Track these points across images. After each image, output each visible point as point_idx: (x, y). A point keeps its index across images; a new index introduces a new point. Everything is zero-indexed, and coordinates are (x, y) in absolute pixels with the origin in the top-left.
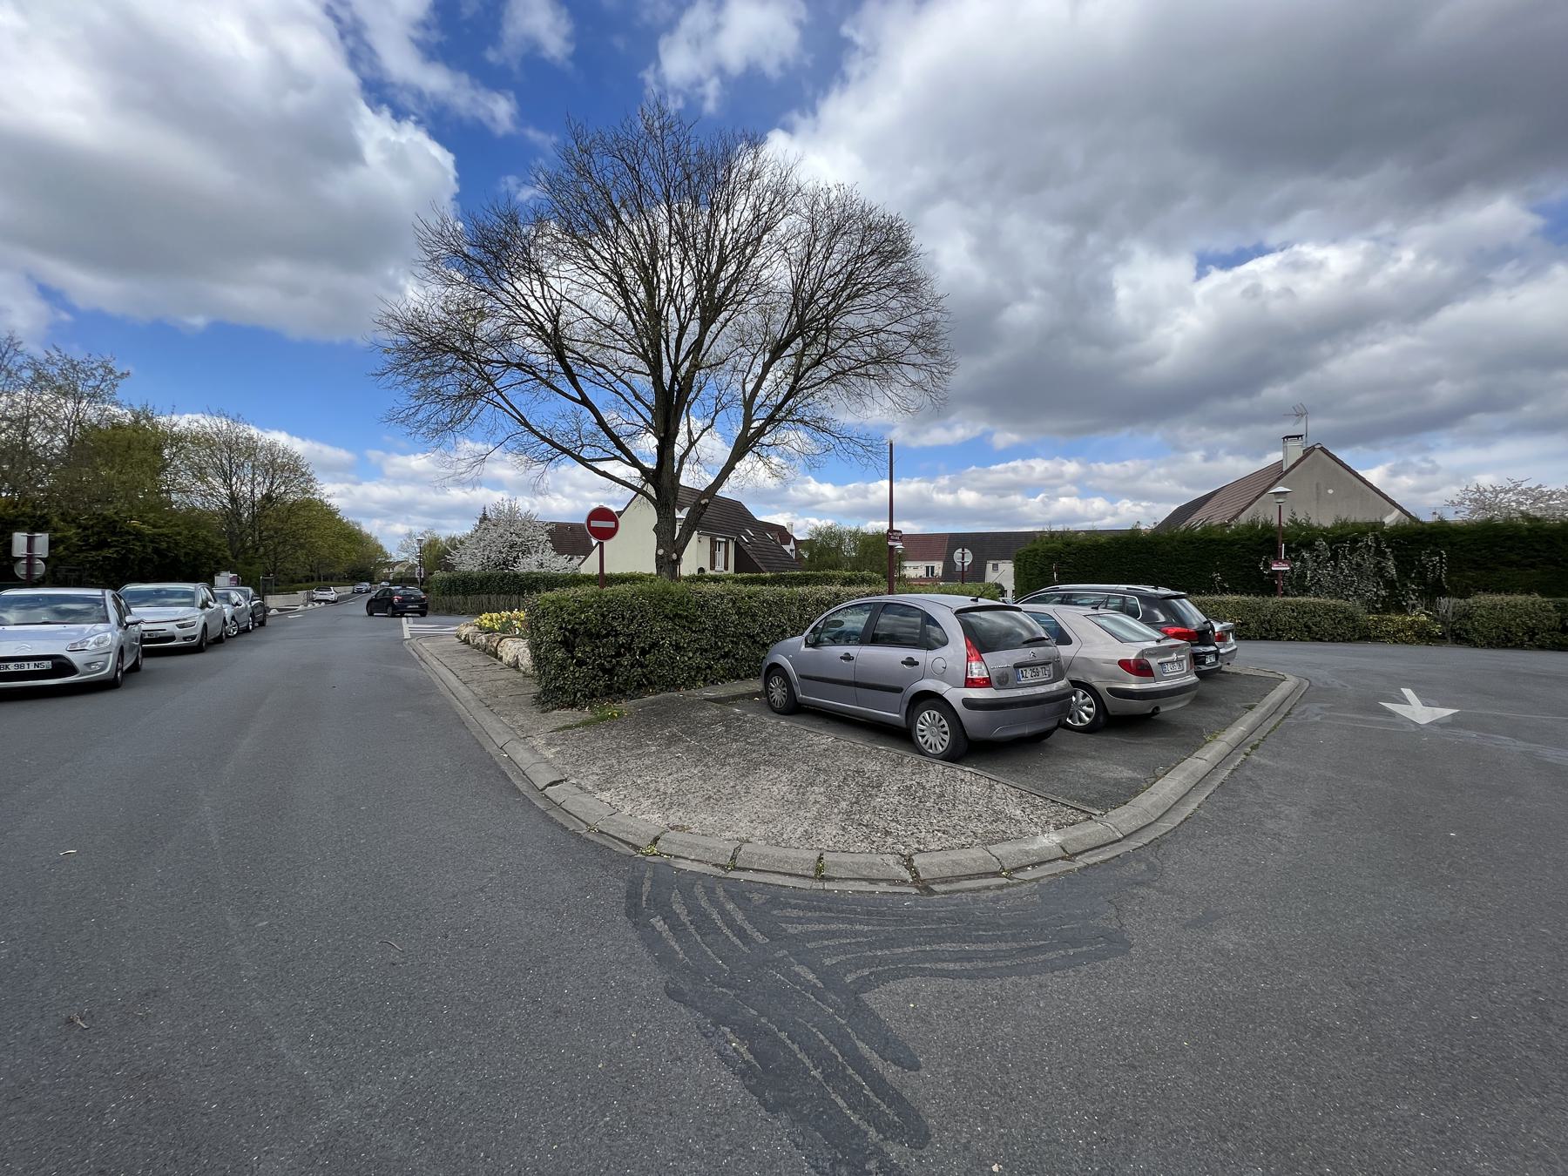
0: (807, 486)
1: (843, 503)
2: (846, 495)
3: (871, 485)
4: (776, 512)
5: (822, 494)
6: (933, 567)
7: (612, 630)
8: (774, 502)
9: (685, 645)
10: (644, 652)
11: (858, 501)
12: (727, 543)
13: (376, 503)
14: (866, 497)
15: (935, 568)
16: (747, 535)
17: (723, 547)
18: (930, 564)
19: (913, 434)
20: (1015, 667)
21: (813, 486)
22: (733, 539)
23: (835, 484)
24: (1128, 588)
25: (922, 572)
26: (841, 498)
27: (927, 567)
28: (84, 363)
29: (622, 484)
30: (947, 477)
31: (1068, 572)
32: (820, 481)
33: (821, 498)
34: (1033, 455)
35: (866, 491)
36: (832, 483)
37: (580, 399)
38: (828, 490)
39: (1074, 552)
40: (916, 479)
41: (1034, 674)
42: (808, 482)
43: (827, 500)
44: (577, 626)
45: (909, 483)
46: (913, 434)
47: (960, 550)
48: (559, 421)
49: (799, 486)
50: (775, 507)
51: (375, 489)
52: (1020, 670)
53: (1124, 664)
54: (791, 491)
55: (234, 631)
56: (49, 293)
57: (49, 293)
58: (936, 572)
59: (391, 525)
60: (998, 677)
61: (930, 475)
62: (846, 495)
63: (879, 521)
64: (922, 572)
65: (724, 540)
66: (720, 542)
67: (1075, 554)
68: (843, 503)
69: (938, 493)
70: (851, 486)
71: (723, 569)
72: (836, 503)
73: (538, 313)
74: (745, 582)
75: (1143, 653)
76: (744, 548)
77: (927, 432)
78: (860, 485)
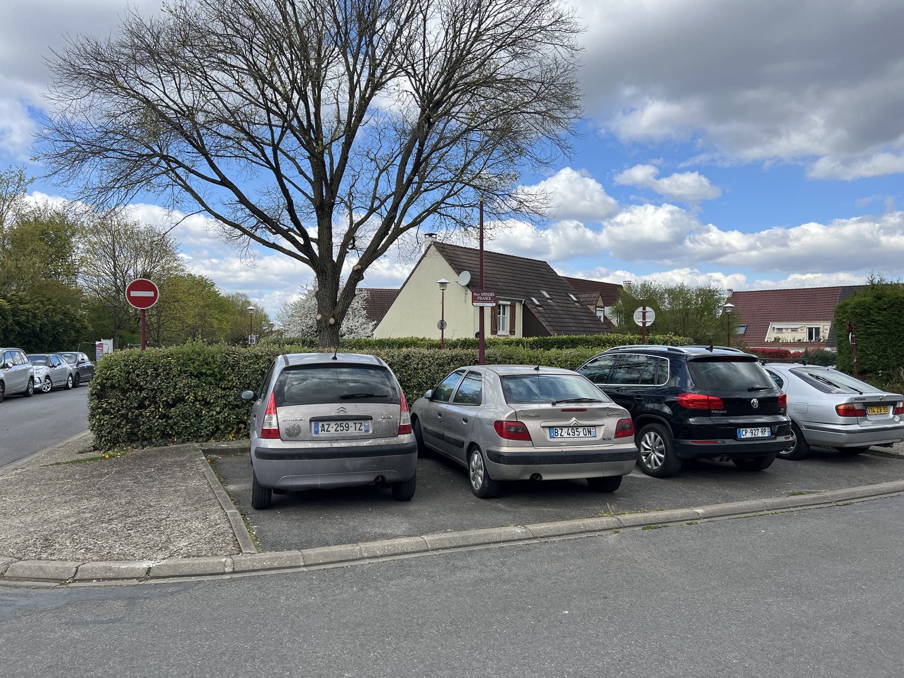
0: (706, 235)
1: (754, 253)
2: (758, 244)
3: (794, 231)
4: (671, 268)
5: (728, 244)
6: (818, 330)
7: (136, 385)
8: (668, 257)
9: (212, 401)
10: (169, 406)
11: (774, 250)
12: (513, 307)
13: (276, 275)
14: (785, 245)
15: (821, 330)
16: (541, 298)
17: (508, 310)
18: (814, 325)
19: (846, 163)
20: (311, 421)
21: (715, 235)
22: (521, 302)
23: (744, 231)
24: (669, 349)
25: (803, 336)
26: (752, 248)
27: (810, 330)
28: (7, 173)
29: (287, 254)
30: (898, 213)
31: (879, 333)
32: (725, 227)
33: (726, 249)
34: (319, 226)
35: (786, 237)
36: (739, 230)
37: (219, 180)
38: (735, 239)
39: (885, 307)
40: (854, 219)
41: (339, 429)
42: (708, 231)
43: (733, 251)
44: (105, 381)
45: (844, 224)
46: (846, 163)
47: (641, 309)
48: (264, 198)
49: (697, 237)
50: (668, 262)
51: (274, 262)
52: (320, 424)
53: (498, 425)
54: (688, 243)
55: (48, 388)
56: (35, 113)
57: (35, 113)
58: (821, 334)
59: (290, 295)
60: (287, 429)
61: (874, 212)
62: (758, 244)
63: (804, 274)
64: (803, 336)
65: (509, 303)
66: (504, 306)
67: (885, 310)
68: (754, 253)
69: (884, 234)
70: (764, 233)
71: (508, 333)
72: (745, 253)
73: (360, 86)
74: (533, 346)
75: (516, 414)
76: (533, 311)
77: (867, 158)
78: (778, 231)
